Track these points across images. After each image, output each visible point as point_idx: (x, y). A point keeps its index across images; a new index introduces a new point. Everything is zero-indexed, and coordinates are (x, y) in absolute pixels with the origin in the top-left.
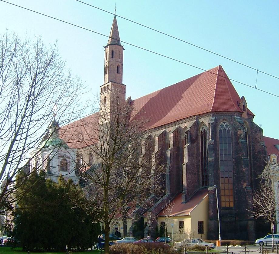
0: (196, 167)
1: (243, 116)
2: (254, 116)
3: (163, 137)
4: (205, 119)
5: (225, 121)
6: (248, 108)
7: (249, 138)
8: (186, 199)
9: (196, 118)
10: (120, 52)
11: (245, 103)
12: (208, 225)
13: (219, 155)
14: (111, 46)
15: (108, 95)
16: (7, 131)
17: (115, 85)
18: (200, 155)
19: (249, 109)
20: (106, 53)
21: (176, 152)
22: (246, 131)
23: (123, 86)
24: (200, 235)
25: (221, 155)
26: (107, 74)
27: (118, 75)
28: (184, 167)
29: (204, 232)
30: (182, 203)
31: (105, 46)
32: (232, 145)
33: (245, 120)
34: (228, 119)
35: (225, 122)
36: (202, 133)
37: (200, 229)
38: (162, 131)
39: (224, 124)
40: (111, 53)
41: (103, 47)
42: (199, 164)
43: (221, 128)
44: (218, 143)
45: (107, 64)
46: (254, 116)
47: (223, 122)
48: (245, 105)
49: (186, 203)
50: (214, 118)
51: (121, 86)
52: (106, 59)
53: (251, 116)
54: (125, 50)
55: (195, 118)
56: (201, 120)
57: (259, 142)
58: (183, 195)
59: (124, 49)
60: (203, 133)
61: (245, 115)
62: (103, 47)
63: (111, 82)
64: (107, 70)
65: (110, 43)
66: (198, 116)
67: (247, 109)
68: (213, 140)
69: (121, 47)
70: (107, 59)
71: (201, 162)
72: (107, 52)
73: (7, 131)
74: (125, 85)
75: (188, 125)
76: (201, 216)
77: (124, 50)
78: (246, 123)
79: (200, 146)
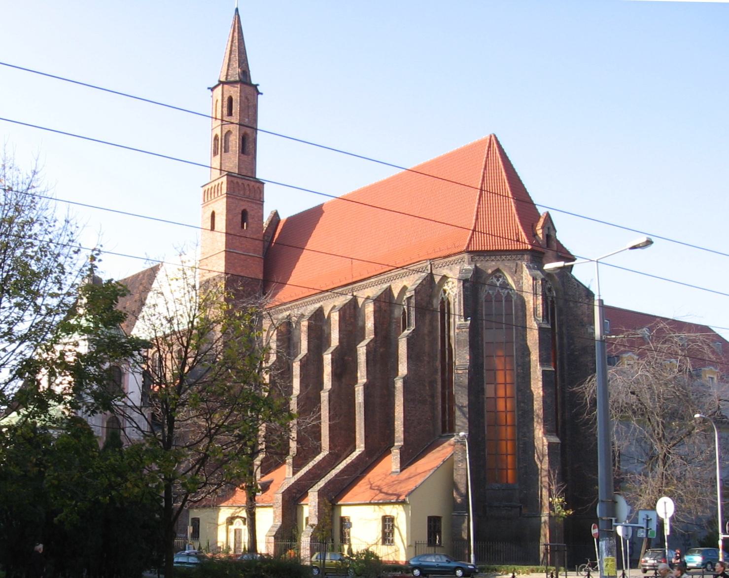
0: (427, 385)
3: (351, 311)
4: (451, 270)
6: (558, 242)
7: (559, 315)
14: (226, 86)
15: (220, 206)
18: (439, 356)
20: (215, 102)
26: (218, 157)
27: (244, 157)
28: (399, 384)
31: (212, 86)
39: (498, 280)
41: (209, 88)
47: (496, 277)
48: (552, 233)
54: (262, 94)
62: (209, 88)
64: (220, 145)
65: (223, 79)
68: (469, 322)
71: (440, 374)
72: (217, 101)
77: (259, 96)
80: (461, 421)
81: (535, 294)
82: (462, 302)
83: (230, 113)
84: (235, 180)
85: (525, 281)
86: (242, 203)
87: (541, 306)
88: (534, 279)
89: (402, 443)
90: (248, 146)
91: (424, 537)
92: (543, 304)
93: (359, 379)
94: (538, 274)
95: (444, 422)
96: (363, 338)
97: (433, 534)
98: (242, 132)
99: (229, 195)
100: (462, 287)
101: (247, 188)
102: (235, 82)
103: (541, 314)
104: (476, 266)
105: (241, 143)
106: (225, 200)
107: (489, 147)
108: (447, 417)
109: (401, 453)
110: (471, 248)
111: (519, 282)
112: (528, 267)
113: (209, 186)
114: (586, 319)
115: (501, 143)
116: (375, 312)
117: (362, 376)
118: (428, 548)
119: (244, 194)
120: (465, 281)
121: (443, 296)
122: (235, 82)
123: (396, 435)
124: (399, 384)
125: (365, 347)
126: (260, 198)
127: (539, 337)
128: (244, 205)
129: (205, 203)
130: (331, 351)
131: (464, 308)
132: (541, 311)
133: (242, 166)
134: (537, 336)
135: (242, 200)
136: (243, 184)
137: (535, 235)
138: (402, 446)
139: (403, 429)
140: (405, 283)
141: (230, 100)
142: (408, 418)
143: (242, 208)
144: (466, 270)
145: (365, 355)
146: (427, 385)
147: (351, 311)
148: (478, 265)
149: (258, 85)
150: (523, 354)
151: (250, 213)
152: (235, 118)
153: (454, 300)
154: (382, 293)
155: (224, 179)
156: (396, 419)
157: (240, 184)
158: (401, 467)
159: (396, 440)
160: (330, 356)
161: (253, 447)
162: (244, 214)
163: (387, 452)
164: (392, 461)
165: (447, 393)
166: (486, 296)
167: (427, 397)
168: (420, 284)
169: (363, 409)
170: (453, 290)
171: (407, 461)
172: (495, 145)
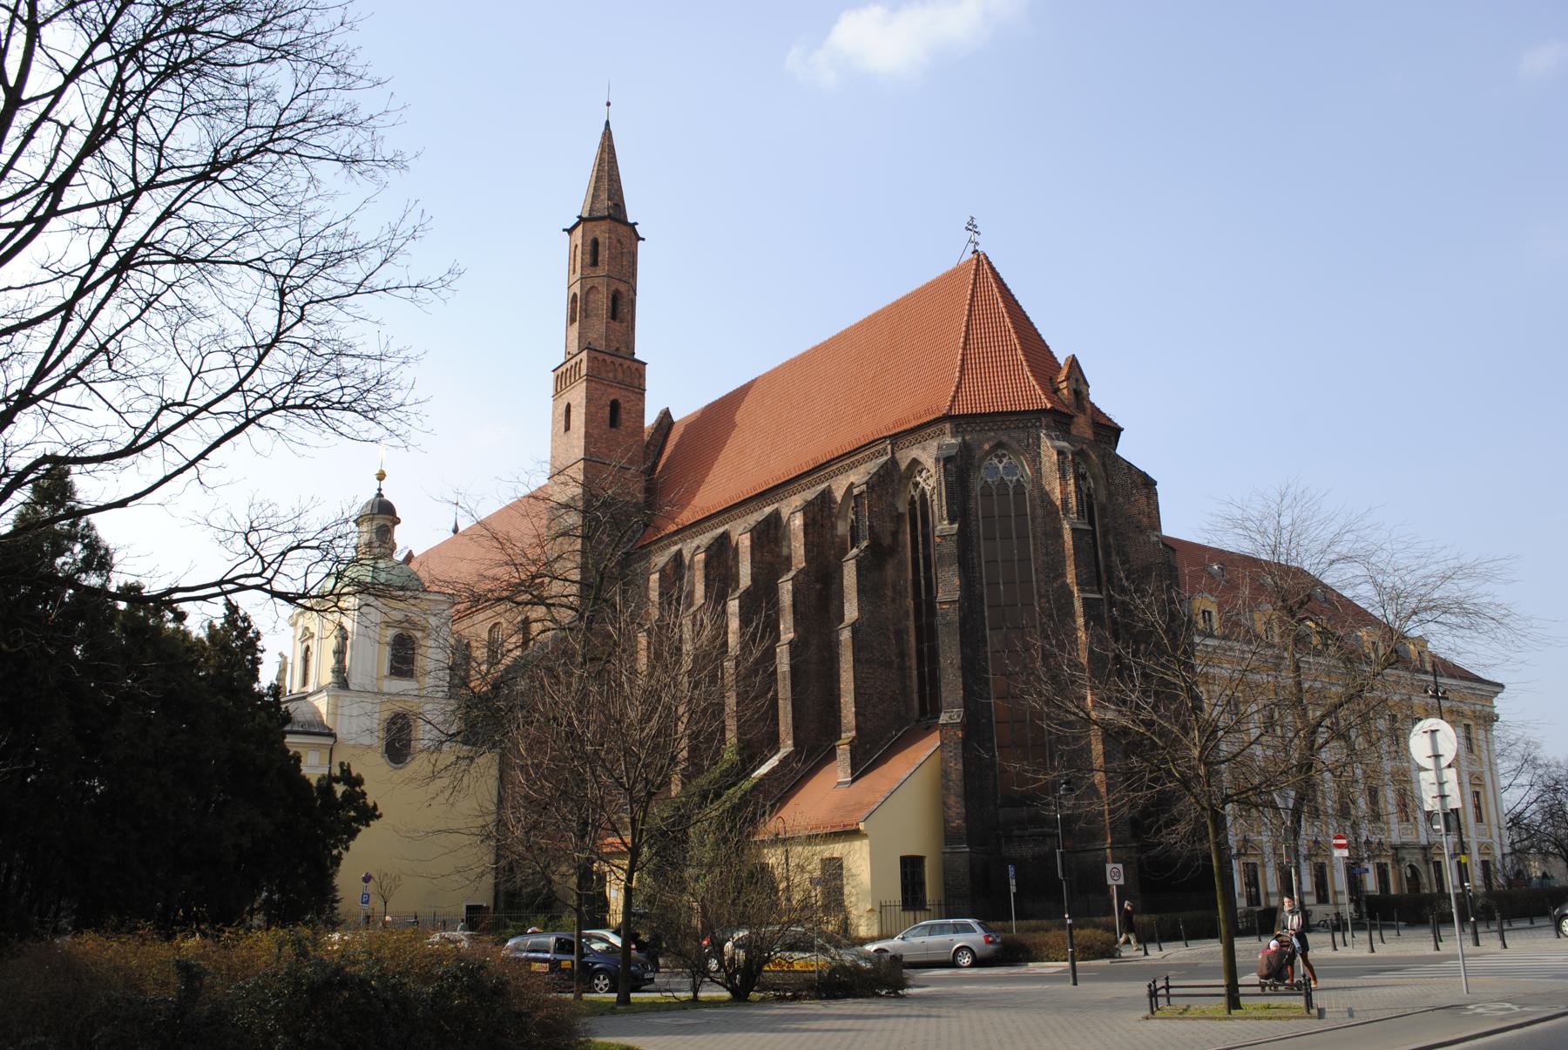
0: (892, 637)
1: (1074, 432)
2: (1117, 431)
3: (769, 534)
4: (924, 449)
5: (1005, 452)
6: (1093, 404)
7: (1102, 517)
8: (854, 766)
9: (889, 447)
10: (621, 244)
11: (1081, 379)
12: (947, 871)
13: (981, 584)
14: (589, 225)
15: (578, 395)
16: (187, 394)
17: (604, 360)
18: (910, 589)
19: (1097, 405)
20: (573, 249)
21: (818, 586)
22: (1089, 489)
23: (636, 365)
24: (907, 913)
25: (993, 584)
26: (577, 324)
27: (616, 325)
28: (846, 636)
29: (925, 901)
30: (839, 783)
31: (569, 227)
32: (1035, 544)
33: (1085, 447)
34: (1014, 444)
35: (1004, 455)
36: (912, 502)
37: (910, 888)
38: (768, 510)
39: (1000, 462)
40: (588, 249)
41: (564, 230)
42: (908, 628)
43: (989, 480)
44: (979, 538)
45: (577, 289)
46: (1117, 431)
47: (996, 456)
48: (1083, 387)
49: (853, 781)
50: (960, 439)
51: (617, 364)
52: (571, 272)
53: (1110, 432)
54: (643, 239)
55: (885, 449)
56: (905, 457)
57: (1141, 531)
58: (843, 751)
59: (641, 236)
60: (918, 507)
61: (1082, 427)
62: (564, 230)
63: (587, 348)
64: (579, 309)
65: (585, 215)
66: (896, 438)
67: (1088, 406)
68: (956, 526)
69: (625, 228)
70: (574, 271)
71: (912, 618)
72: (576, 246)
73: (187, 394)
74: (645, 364)
75: (857, 477)
76: (915, 836)
77: (640, 242)
78: (1089, 456)
79: (909, 554)
80: (950, 716)
81: (1063, 477)
82: (944, 494)
83: (595, 263)
84: (601, 357)
85: (1044, 459)
86: (610, 390)
87: (1073, 494)
88: (1060, 452)
89: (853, 733)
90: (621, 307)
91: (895, 893)
92: (1076, 492)
93: (782, 633)
94: (1065, 447)
95: (922, 699)
96: (789, 570)
97: (910, 888)
98: (613, 288)
99: (590, 377)
100: (942, 470)
101: (619, 369)
102: (602, 218)
103: (1075, 508)
104: (964, 439)
105: (610, 304)
106: (585, 384)
107: (977, 270)
108: (928, 688)
109: (851, 751)
110: (955, 412)
111: (1034, 461)
112: (1048, 436)
113: (563, 369)
114: (1145, 520)
115: (994, 264)
116: (806, 525)
117: (786, 629)
118: (902, 913)
119: (615, 377)
120: (948, 460)
121: (913, 493)
122: (602, 218)
123: (844, 721)
124: (846, 636)
125: (748, 535)
126: (640, 384)
127: (1074, 545)
128: (615, 393)
129: (558, 393)
130: (738, 595)
131: (947, 503)
132: (1074, 503)
133: (612, 337)
134: (1071, 543)
135: (612, 386)
136: (612, 362)
137: (1056, 390)
138: (854, 738)
139: (854, 709)
140: (853, 478)
141: (595, 243)
142: (862, 691)
143: (613, 397)
144: (948, 445)
145: (791, 595)
146: (892, 637)
147: (769, 534)
148: (967, 438)
149: (636, 224)
150: (1048, 577)
151: (624, 405)
152: (602, 270)
153: (931, 497)
154: (816, 498)
155: (584, 355)
156: (842, 693)
157: (608, 362)
158: (852, 774)
159: (843, 728)
160: (736, 602)
161: (673, 758)
162: (615, 407)
163: (831, 756)
164: (840, 770)
165: (925, 649)
166: (982, 488)
167: (893, 658)
168: (875, 474)
169: (788, 682)
170: (930, 480)
171: (862, 766)
172: (986, 266)
